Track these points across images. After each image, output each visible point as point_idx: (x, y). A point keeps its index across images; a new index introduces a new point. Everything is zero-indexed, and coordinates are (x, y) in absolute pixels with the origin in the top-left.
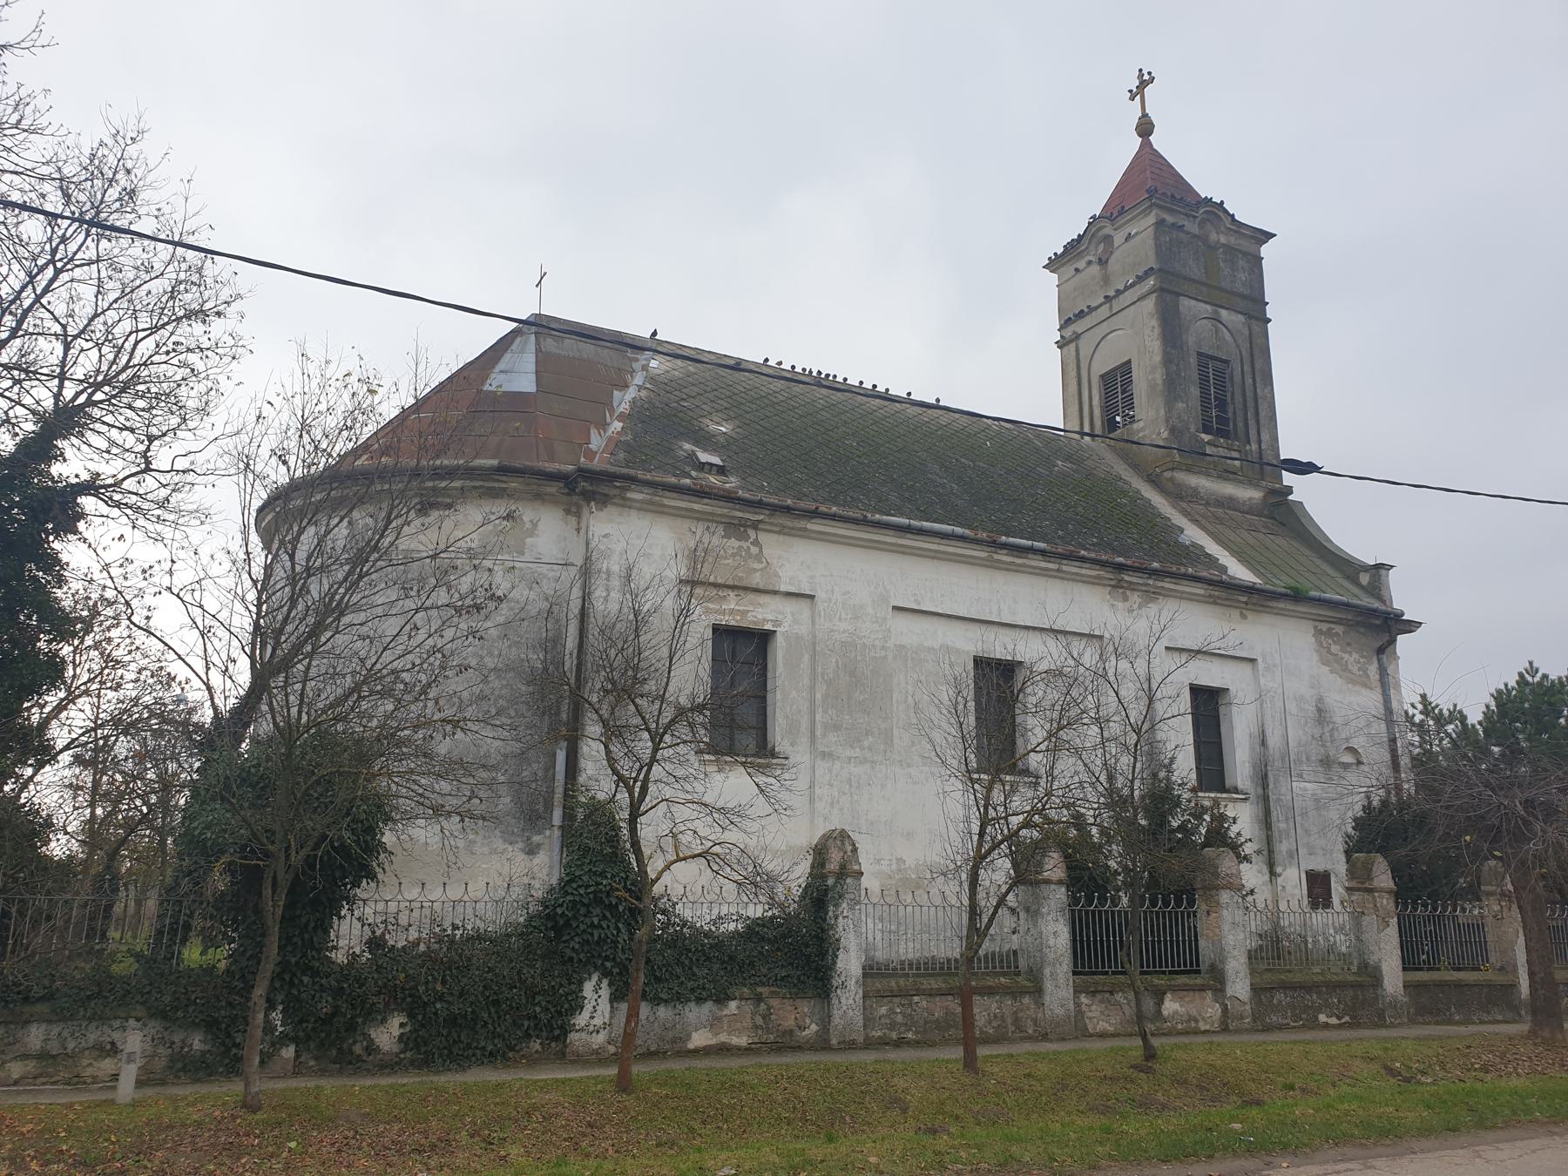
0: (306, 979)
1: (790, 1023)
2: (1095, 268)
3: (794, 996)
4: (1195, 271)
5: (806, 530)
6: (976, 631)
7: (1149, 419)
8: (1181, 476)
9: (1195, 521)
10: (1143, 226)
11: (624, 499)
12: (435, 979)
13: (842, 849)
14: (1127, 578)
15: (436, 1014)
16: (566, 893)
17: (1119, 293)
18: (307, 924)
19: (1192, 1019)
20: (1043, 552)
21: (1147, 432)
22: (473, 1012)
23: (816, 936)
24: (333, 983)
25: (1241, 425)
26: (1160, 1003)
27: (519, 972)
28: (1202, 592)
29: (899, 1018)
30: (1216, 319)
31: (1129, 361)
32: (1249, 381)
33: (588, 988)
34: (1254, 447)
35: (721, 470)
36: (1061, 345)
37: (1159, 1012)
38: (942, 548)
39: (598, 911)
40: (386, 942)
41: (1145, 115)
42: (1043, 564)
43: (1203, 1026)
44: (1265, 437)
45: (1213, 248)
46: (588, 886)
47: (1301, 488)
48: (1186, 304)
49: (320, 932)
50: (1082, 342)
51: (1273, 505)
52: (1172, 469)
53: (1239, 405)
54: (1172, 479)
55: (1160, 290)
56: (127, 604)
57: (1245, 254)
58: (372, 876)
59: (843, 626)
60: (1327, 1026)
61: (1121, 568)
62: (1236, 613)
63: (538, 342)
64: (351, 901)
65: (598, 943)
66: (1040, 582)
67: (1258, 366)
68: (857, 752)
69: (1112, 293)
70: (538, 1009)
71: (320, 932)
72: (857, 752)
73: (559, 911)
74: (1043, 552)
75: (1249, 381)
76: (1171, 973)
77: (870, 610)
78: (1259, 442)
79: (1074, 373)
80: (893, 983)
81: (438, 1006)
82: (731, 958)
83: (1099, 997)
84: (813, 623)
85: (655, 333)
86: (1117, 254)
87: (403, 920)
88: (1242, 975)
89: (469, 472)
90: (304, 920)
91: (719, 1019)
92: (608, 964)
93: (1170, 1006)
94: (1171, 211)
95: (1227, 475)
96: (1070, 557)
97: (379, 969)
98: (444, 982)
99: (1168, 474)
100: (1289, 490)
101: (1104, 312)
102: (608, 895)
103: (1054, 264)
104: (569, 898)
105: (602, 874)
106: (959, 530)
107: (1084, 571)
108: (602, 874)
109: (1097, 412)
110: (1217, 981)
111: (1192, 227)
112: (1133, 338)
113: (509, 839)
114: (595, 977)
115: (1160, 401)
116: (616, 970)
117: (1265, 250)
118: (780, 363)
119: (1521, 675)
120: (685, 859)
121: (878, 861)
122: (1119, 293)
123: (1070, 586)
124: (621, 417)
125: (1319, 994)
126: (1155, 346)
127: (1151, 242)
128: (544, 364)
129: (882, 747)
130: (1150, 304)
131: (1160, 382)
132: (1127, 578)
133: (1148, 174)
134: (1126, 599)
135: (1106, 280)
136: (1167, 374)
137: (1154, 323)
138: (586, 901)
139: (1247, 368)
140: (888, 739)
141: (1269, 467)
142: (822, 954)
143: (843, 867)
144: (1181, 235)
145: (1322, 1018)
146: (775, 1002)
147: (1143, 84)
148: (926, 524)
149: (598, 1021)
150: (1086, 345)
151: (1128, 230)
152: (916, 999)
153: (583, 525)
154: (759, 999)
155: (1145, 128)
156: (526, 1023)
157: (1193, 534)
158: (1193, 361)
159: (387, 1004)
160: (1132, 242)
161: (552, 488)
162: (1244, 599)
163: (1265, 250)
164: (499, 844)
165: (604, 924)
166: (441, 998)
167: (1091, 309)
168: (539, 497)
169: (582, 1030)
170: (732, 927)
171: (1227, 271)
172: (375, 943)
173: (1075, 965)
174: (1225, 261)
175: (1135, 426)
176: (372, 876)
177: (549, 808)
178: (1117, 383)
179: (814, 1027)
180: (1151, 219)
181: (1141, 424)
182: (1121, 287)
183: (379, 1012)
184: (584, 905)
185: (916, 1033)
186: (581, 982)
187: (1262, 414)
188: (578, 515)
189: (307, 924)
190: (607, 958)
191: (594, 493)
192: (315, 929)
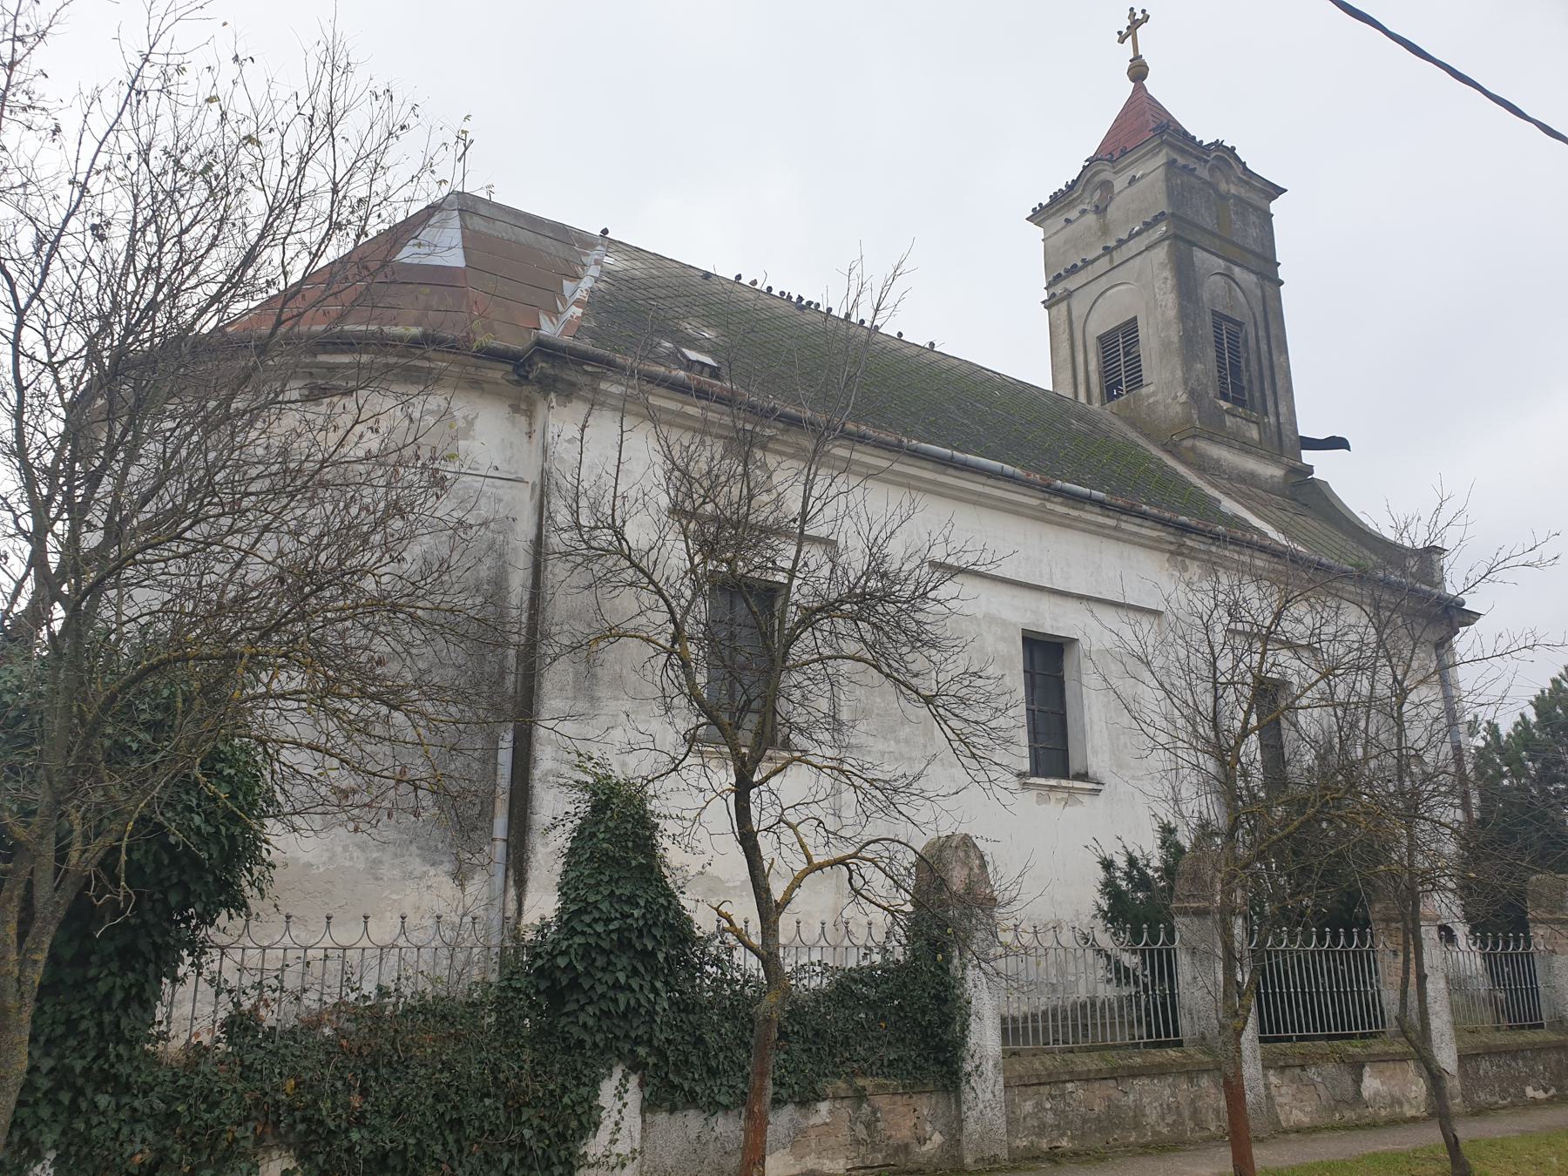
0: (103, 1100)
1: (904, 1133)
2: (1091, 218)
3: (909, 1091)
4: (1208, 221)
6: (1028, 598)
7: (1164, 383)
8: (1205, 447)
9: (1227, 494)
10: (1151, 169)
11: (596, 390)
12: (349, 1088)
13: (965, 864)
14: (1189, 543)
15: (350, 1150)
16: (573, 932)
17: (1121, 242)
18: (109, 995)
19: (1396, 1101)
20: (1101, 504)
21: (1159, 397)
22: (419, 1143)
23: (937, 997)
24: (160, 1106)
25: (1257, 394)
26: (1358, 1081)
27: (496, 1069)
29: (1050, 1118)
30: (1228, 276)
32: (1264, 347)
33: (607, 1089)
34: (1272, 420)
35: (715, 373)
36: (1049, 304)
37: (1358, 1093)
38: (988, 490)
39: (623, 961)
40: (259, 1022)
42: (1101, 519)
43: (1410, 1112)
44: (1283, 409)
45: (1224, 197)
46: (609, 920)
47: (1321, 464)
48: (1199, 255)
49: (135, 1007)
50: (1074, 302)
51: (1293, 485)
52: (1194, 437)
53: (1255, 373)
54: (1193, 449)
55: (1174, 238)
57: (1256, 209)
58: (238, 903)
60: (1535, 1102)
61: (1184, 529)
63: (462, 219)
64: (198, 949)
65: (624, 1015)
66: (1094, 542)
67: (1273, 332)
68: (892, 746)
69: (1112, 244)
70: (527, 1133)
71: (135, 1007)
72: (892, 746)
73: (562, 962)
74: (1101, 504)
75: (1264, 347)
76: (1363, 1036)
78: (1277, 415)
79: (1064, 337)
80: (1037, 1065)
81: (355, 1136)
82: (817, 1034)
83: (1288, 1072)
85: (605, 231)
86: (1118, 200)
87: (292, 981)
88: (1447, 1038)
89: (383, 343)
90: (102, 987)
91: (803, 1132)
92: (642, 1051)
93: (1371, 1084)
94: (1182, 151)
95: (1246, 447)
96: (1130, 512)
97: (247, 1072)
98: (364, 1092)
99: (1188, 443)
100: (1310, 469)
101: (1103, 264)
102: (640, 936)
103: (1039, 216)
104: (579, 940)
105: (632, 901)
106: (1008, 468)
107: (1144, 531)
108: (632, 901)
109: (1094, 378)
110: (1419, 1051)
111: (1203, 172)
112: (1142, 293)
113: (431, 857)
114: (618, 1073)
115: (1176, 361)
116: (651, 1060)
117: (1274, 207)
118: (754, 283)
119: (1554, 681)
120: (820, 867)
122: (1121, 242)
123: (1127, 549)
124: (578, 303)
125: (1524, 1058)
126: (1168, 300)
127: (1161, 185)
128: (471, 242)
129: (921, 740)
130: (1161, 253)
131: (1176, 339)
132: (1189, 543)
133: (1148, 116)
135: (1105, 230)
136: (1185, 330)
137: (1167, 273)
138: (606, 945)
139: (1261, 333)
141: (1286, 443)
142: (946, 1022)
143: (969, 889)
144: (1193, 179)
145: (1530, 1092)
146: (881, 1101)
147: (1135, 24)
148: (972, 458)
149: (622, 1148)
150: (1079, 305)
151: (1132, 173)
152: (1070, 1086)
153: (538, 427)
154: (860, 1096)
155: (1138, 71)
156: (506, 1157)
157: (1229, 506)
158: (1208, 319)
159: (259, 1140)
160: (1137, 185)
161: (497, 373)
163: (1274, 207)
164: (417, 865)
165: (635, 984)
166: (360, 1121)
167: (1086, 263)
168: (476, 385)
169: (597, 1164)
170: (814, 983)
171: (1239, 225)
172: (239, 1025)
173: (1263, 1031)
174: (1236, 213)
175: (1144, 391)
176: (238, 903)
177: (487, 814)
178: (1119, 348)
179: (937, 1138)
180: (1161, 159)
181: (1152, 388)
182: (1124, 236)
183: (244, 1155)
184: (603, 951)
185: (1072, 1138)
186: (595, 1084)
187: (1279, 383)
188: (530, 415)
189: (109, 995)
190: (638, 1041)
191: (556, 379)
192: (125, 1005)
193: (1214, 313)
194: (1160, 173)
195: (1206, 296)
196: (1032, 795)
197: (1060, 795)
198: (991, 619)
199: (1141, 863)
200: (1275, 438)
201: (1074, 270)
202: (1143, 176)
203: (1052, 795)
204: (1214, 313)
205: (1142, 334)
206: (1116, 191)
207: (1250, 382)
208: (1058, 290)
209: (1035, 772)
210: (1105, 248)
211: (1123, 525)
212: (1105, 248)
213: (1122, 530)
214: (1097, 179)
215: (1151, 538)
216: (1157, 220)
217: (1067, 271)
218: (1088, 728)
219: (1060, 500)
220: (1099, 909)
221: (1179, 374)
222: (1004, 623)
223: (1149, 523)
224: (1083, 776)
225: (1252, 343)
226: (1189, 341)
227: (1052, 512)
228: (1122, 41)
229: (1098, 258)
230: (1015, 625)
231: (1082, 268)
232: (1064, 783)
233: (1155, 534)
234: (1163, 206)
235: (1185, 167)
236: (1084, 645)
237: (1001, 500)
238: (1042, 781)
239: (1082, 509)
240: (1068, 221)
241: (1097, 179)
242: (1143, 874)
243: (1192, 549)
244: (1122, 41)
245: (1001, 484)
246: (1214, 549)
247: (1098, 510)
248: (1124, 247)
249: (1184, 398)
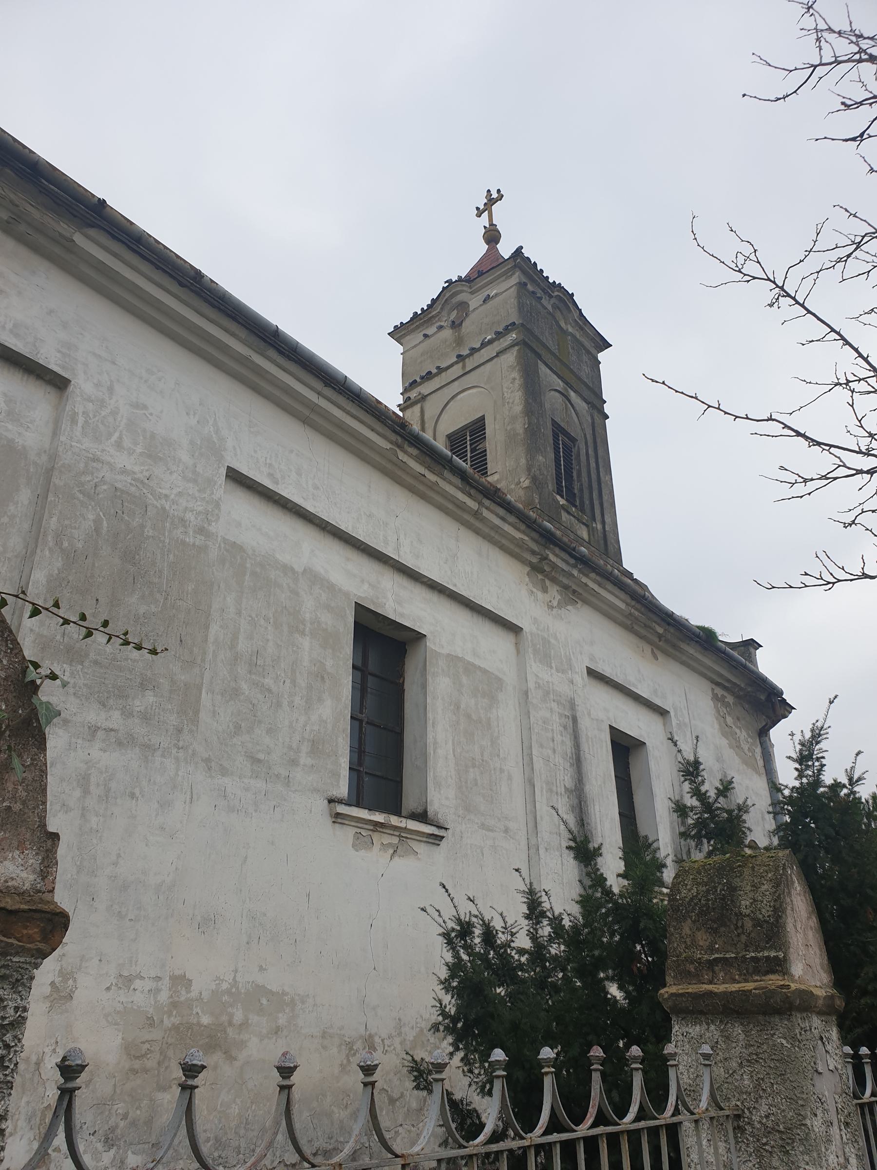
2: (447, 333)
5: (68, 245)
14: (552, 557)
17: (473, 351)
25: (587, 502)
28: (622, 606)
31: (482, 418)
32: (593, 465)
34: (599, 527)
41: (492, 224)
42: (461, 496)
44: (608, 520)
56: (16, 1064)
57: (588, 352)
59: (122, 460)
62: (648, 649)
68: (115, 719)
69: (466, 352)
72: (115, 719)
75: (593, 465)
77: (184, 456)
78: (603, 523)
84: (55, 433)
86: (473, 317)
101: (457, 370)
103: (399, 333)
107: (507, 528)
117: (601, 356)
121: (127, 981)
122: (473, 351)
126: (516, 399)
127: (513, 301)
129: (173, 720)
130: (510, 358)
132: (552, 557)
134: (545, 590)
135: (459, 341)
136: (529, 424)
137: (515, 374)
139: (591, 452)
140: (188, 703)
147: (491, 201)
160: (491, 303)
162: (660, 630)
163: (601, 356)
167: (441, 371)
171: (574, 358)
174: (573, 348)
181: (496, 477)
182: (477, 346)
187: (605, 498)
193: (554, 423)
194: (513, 291)
195: (547, 406)
196: (348, 833)
197: (387, 839)
198: (314, 578)
199: (502, 938)
200: (602, 542)
201: (429, 376)
202: (496, 295)
203: (376, 837)
204: (554, 423)
205: (489, 431)
206: (471, 309)
207: (581, 490)
208: (413, 394)
209: (357, 798)
210: (459, 356)
211: (486, 513)
212: (459, 356)
213: (483, 520)
214: (455, 300)
215: (512, 539)
216: (507, 330)
217: (422, 378)
218: (430, 750)
219: (414, 452)
220: (444, 1014)
221: (523, 461)
222: (331, 588)
223: (512, 519)
224: (422, 817)
225: (583, 458)
226: (532, 432)
227: (403, 466)
228: (479, 215)
229: (452, 365)
230: (347, 595)
231: (436, 375)
232: (394, 820)
233: (518, 535)
234: (514, 318)
235: (533, 292)
236: (430, 644)
237: (341, 426)
238: (363, 814)
239: (440, 475)
240: (426, 336)
241: (455, 300)
242: (504, 958)
243: (554, 566)
244: (479, 215)
245: (341, 400)
246: (575, 572)
247: (457, 481)
248: (476, 355)
249: (527, 483)
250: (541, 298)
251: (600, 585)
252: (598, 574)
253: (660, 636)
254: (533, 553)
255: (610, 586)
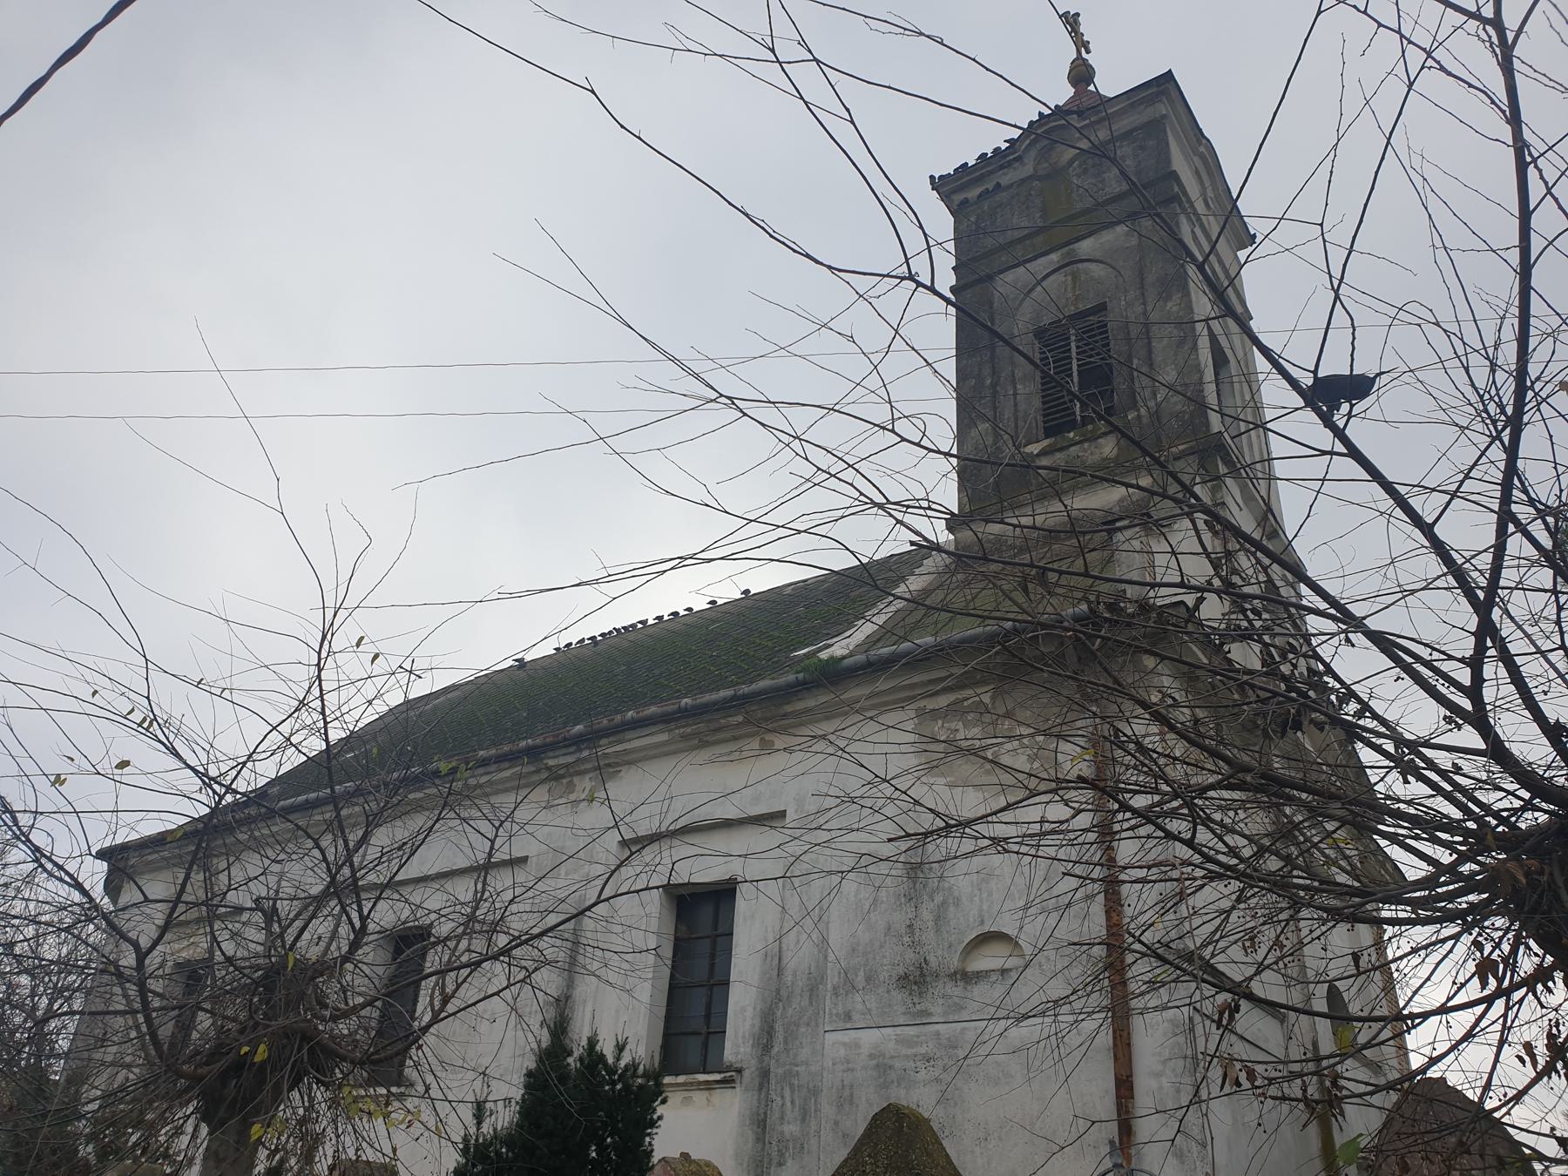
28: (664, 737)
132: (551, 762)
215: (508, 779)
233: (507, 773)
250: (998, 185)
251: (620, 742)
252: (607, 736)
253: (747, 722)
254: (538, 771)
255: (629, 735)
